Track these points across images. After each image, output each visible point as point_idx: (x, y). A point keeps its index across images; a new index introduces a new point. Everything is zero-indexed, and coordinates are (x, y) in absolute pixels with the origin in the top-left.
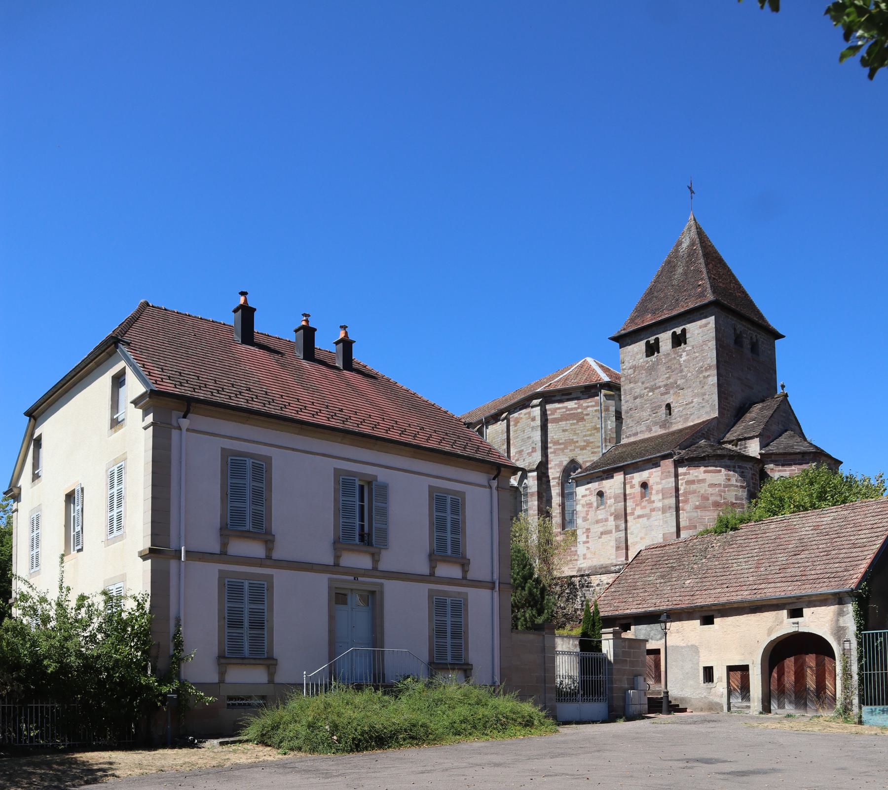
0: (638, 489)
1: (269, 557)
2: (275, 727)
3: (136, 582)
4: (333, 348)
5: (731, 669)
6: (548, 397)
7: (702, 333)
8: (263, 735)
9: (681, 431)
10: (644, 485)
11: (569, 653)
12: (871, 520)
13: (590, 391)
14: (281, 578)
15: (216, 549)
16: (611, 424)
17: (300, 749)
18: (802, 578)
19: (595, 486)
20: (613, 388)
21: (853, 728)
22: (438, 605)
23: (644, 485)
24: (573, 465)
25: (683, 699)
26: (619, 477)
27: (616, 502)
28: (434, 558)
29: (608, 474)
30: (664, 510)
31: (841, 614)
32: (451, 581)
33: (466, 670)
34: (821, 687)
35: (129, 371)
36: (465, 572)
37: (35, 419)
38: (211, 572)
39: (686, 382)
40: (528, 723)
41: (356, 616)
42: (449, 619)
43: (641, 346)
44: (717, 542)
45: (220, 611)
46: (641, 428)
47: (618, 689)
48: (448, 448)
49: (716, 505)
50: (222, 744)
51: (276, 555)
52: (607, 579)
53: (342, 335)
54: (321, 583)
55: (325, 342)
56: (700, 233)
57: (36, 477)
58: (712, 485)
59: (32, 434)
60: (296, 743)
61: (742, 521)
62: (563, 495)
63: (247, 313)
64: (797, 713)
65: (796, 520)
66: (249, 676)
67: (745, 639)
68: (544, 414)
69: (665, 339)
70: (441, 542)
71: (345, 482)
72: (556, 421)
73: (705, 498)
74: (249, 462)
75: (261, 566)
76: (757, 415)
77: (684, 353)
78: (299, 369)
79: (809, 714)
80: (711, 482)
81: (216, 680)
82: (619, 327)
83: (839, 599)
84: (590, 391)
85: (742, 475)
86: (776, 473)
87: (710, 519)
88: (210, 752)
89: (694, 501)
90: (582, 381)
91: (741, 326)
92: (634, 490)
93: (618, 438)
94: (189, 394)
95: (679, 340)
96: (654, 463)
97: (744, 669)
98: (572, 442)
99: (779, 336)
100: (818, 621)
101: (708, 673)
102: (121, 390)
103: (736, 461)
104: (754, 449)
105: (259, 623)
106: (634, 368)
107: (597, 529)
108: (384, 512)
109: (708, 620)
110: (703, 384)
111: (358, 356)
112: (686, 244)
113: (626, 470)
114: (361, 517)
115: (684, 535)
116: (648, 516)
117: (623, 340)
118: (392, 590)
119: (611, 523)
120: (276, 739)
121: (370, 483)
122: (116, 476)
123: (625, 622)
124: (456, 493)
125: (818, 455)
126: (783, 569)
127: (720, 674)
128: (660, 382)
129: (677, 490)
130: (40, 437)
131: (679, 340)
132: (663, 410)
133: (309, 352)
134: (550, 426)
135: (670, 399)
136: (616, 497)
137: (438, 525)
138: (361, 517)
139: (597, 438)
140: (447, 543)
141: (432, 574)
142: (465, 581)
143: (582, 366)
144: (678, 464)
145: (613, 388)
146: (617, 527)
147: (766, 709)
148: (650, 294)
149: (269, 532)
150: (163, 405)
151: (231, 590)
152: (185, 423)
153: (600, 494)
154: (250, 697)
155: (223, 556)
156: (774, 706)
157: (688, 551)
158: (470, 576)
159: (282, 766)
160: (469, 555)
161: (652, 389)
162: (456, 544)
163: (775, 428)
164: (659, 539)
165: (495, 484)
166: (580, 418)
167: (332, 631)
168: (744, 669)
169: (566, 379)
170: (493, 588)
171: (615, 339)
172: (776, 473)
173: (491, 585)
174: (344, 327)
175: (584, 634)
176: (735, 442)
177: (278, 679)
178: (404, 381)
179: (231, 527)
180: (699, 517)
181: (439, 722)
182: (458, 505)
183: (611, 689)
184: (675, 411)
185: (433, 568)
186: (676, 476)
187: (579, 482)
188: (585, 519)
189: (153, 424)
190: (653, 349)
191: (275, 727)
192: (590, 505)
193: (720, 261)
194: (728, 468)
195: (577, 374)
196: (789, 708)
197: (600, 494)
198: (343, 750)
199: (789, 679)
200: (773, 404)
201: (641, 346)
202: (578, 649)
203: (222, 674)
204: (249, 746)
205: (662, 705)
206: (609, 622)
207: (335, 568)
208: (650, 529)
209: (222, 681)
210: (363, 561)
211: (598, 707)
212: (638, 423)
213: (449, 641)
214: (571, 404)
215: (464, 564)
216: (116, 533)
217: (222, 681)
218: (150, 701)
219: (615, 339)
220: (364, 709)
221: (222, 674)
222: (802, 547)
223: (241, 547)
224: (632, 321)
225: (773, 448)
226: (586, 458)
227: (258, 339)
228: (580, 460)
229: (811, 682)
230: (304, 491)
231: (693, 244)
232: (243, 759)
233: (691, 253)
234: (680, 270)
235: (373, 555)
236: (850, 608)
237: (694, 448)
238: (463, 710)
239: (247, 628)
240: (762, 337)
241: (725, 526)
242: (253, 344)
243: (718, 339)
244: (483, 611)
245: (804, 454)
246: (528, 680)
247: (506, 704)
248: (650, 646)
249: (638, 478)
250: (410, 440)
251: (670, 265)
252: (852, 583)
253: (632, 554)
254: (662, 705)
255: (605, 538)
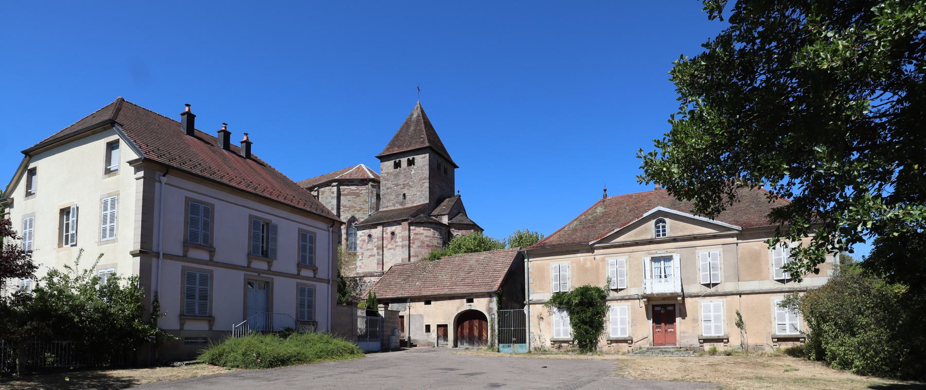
0: (389, 235)
1: (211, 260)
2: (221, 355)
3: (127, 270)
4: (239, 145)
5: (439, 326)
6: (341, 182)
7: (422, 160)
8: (213, 359)
9: (410, 208)
10: (393, 233)
11: (363, 317)
12: (501, 259)
13: (364, 182)
14: (218, 272)
15: (181, 253)
16: (374, 200)
17: (238, 367)
18: (472, 284)
19: (367, 231)
20: (376, 182)
21: (497, 354)
22: (301, 291)
23: (393, 233)
24: (353, 219)
25: (415, 341)
26: (380, 228)
27: (378, 240)
28: (300, 266)
29: (375, 226)
30: (403, 247)
31: (490, 302)
32: (308, 278)
33: (315, 323)
34: (480, 335)
35: (122, 142)
36: (315, 274)
37: (30, 157)
38: (177, 266)
39: (413, 184)
40: (352, 353)
41: (259, 296)
42: (306, 298)
43: (391, 163)
44: (430, 265)
45: (182, 289)
46: (390, 204)
47: (384, 335)
48: (308, 209)
49: (428, 246)
50: (187, 364)
51: (216, 259)
52: (375, 279)
53: (245, 139)
54: (241, 275)
55: (235, 141)
56: (422, 111)
57: (29, 194)
58: (426, 236)
59: (27, 166)
60: (236, 363)
61: (442, 255)
62: (347, 234)
63: (190, 118)
64: (470, 347)
65: (468, 256)
66: (197, 327)
67: (445, 312)
68: (339, 190)
69: (404, 161)
70: (303, 258)
71: (255, 222)
72: (345, 195)
73: (423, 242)
74: (202, 206)
75: (207, 264)
76: (446, 204)
77: (413, 170)
78: (222, 154)
79: (476, 348)
80: (424, 234)
81: (178, 328)
82: (380, 152)
83: (490, 295)
84: (364, 182)
85: (441, 234)
86: (455, 232)
87: (426, 253)
88: (181, 371)
89: (417, 243)
90: (359, 176)
91: (440, 160)
92: (388, 235)
93: (378, 208)
94: (167, 163)
95: (411, 163)
96: (398, 223)
97: (446, 326)
98: (353, 207)
99: (457, 167)
100: (480, 305)
101: (428, 328)
102: (113, 152)
103: (437, 226)
104: (445, 220)
105: (204, 297)
106: (388, 173)
107: (367, 253)
108: (275, 240)
109: (428, 302)
110: (422, 186)
111: (253, 152)
112: (415, 116)
113: (384, 225)
114: (263, 242)
115: (412, 260)
116: (395, 249)
117: (383, 158)
118: (278, 282)
119: (375, 251)
120: (223, 361)
121: (268, 224)
122: (110, 204)
123: (386, 302)
124: (312, 232)
125: (474, 226)
126: (463, 280)
127: (434, 328)
128: (401, 182)
129: (409, 237)
130: (35, 169)
131: (411, 163)
132: (402, 196)
133: (227, 145)
134: (342, 197)
135: (405, 191)
136: (378, 238)
137: (302, 249)
138: (263, 242)
139: (367, 206)
140: (306, 259)
141: (299, 274)
142: (315, 278)
143: (359, 168)
144: (410, 224)
145: (376, 182)
146: (378, 254)
147: (456, 345)
148: (397, 137)
149: (211, 246)
150: (152, 169)
151: (189, 277)
152: (164, 179)
153: (370, 236)
154: (197, 338)
155: (184, 258)
156: (459, 344)
157: (416, 268)
158: (317, 276)
159: (235, 376)
160: (317, 265)
161: (397, 185)
162: (311, 259)
163: (455, 211)
164: (400, 261)
165: (331, 229)
166: (358, 195)
167: (245, 303)
168: (446, 326)
169: (351, 174)
170: (328, 283)
171: (379, 157)
172: (455, 232)
173: (328, 282)
174: (246, 134)
175: (368, 307)
176: (437, 216)
177: (214, 328)
178: (279, 169)
179: (190, 242)
180: (420, 252)
181: (309, 351)
182: (312, 240)
183: (383, 335)
184: (408, 198)
185: (299, 271)
186: (409, 230)
187: (360, 228)
188: (361, 248)
189: (143, 177)
190: (397, 165)
191: (221, 355)
192: (364, 241)
193: (431, 126)
194: (434, 229)
195: (356, 172)
196: (466, 345)
197: (370, 236)
198: (263, 367)
199: (466, 331)
200: (454, 199)
201: (391, 163)
202: (365, 315)
203: (182, 325)
204: (204, 365)
205: (406, 344)
206: (380, 301)
207: (248, 268)
208: (395, 256)
209: (181, 329)
210: (263, 265)
211: (376, 344)
212: (389, 201)
213: (306, 309)
214: (353, 188)
215: (315, 270)
216: (108, 238)
217: (181, 329)
218: (139, 338)
219: (379, 157)
220: (272, 345)
221: (182, 325)
222: (471, 270)
223: (194, 253)
224: (387, 149)
225: (454, 220)
226: (362, 217)
227: (232, 148)
228: (357, 216)
229: (476, 333)
230: (231, 225)
231: (419, 116)
232: (206, 373)
233: (418, 121)
234: (412, 128)
235: (269, 262)
236: (495, 299)
237: (418, 217)
238: (320, 345)
239: (197, 297)
240: (449, 167)
241: (434, 257)
242: (250, 159)
243: (430, 165)
244: (323, 294)
245: (468, 225)
246: (349, 332)
247: (340, 343)
248: (401, 314)
249: (390, 229)
250: (289, 203)
251: (407, 124)
252: (495, 288)
253: (386, 269)
254: (406, 344)
255: (374, 258)
